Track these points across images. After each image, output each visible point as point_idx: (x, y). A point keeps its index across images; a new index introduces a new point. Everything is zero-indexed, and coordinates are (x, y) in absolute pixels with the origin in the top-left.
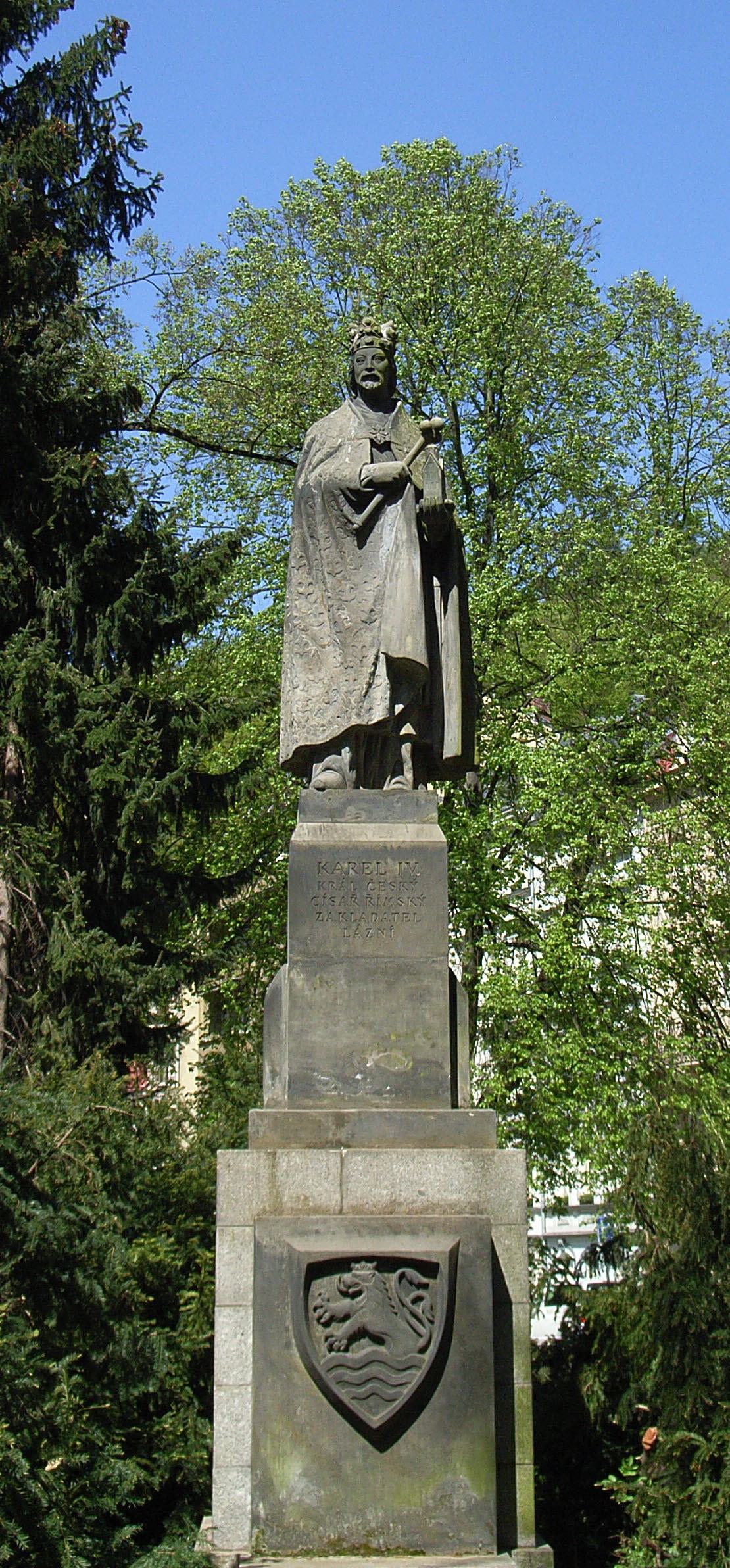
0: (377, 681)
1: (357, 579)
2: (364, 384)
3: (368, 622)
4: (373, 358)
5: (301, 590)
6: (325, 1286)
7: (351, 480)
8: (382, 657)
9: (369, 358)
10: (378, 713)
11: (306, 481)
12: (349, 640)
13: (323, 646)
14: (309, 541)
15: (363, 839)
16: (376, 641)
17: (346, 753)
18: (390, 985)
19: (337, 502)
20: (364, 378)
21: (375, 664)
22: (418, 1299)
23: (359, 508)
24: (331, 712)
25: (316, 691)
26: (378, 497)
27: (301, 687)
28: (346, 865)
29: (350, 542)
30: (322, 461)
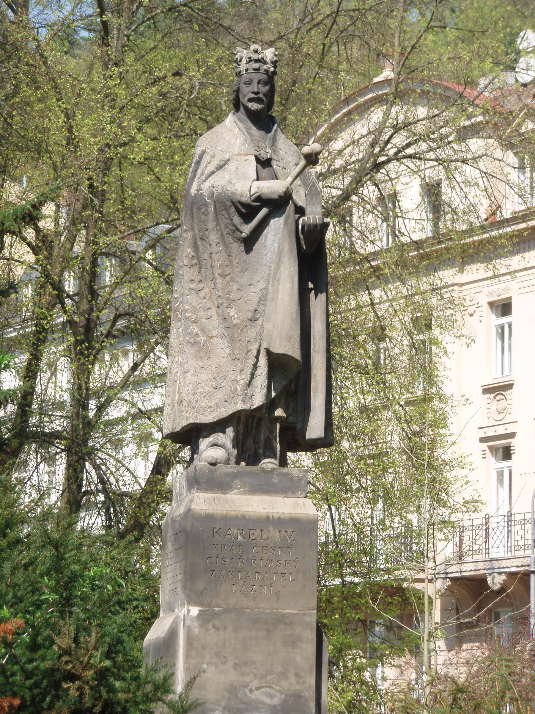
0: (259, 371)
1: (243, 281)
2: (250, 105)
3: (253, 320)
4: (259, 83)
5: (193, 286)
7: (242, 196)
8: (263, 352)
9: (255, 82)
10: (258, 400)
11: (199, 190)
12: (236, 335)
13: (211, 337)
14: (199, 243)
15: (250, 509)
16: (259, 338)
17: (230, 431)
18: (269, 631)
19: (228, 212)
20: (250, 100)
21: (257, 357)
23: (247, 217)
24: (219, 396)
25: (204, 376)
26: (264, 211)
27: (191, 372)
28: (236, 531)
29: (238, 248)
30: (213, 173)
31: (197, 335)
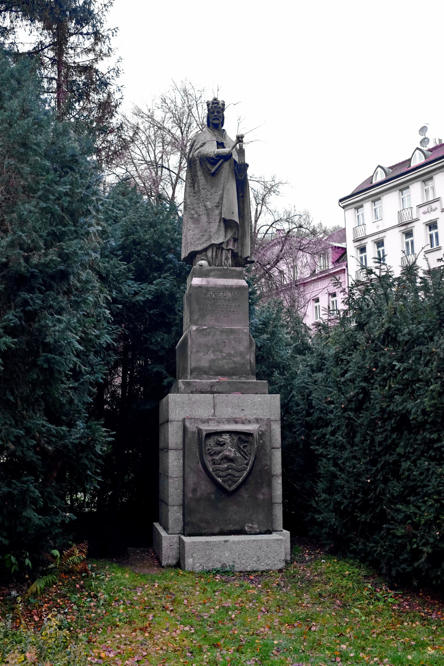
6: (211, 442)
11: (193, 155)
13: (200, 215)
20: (214, 119)
22: (245, 447)
23: (214, 164)
24: (204, 239)
31: (194, 214)
